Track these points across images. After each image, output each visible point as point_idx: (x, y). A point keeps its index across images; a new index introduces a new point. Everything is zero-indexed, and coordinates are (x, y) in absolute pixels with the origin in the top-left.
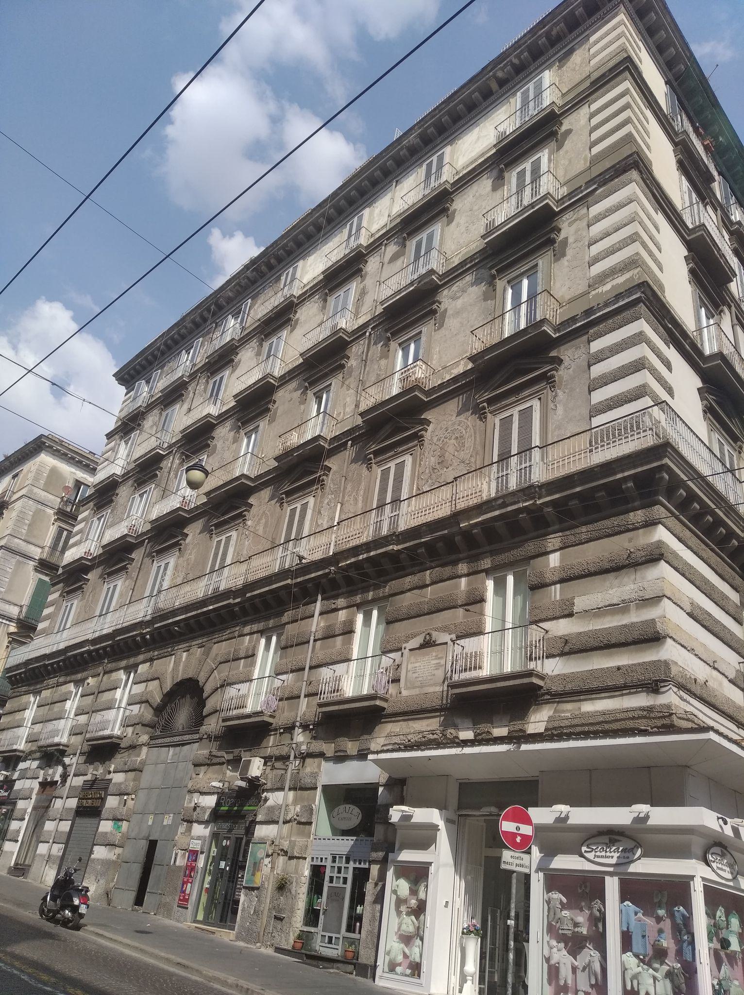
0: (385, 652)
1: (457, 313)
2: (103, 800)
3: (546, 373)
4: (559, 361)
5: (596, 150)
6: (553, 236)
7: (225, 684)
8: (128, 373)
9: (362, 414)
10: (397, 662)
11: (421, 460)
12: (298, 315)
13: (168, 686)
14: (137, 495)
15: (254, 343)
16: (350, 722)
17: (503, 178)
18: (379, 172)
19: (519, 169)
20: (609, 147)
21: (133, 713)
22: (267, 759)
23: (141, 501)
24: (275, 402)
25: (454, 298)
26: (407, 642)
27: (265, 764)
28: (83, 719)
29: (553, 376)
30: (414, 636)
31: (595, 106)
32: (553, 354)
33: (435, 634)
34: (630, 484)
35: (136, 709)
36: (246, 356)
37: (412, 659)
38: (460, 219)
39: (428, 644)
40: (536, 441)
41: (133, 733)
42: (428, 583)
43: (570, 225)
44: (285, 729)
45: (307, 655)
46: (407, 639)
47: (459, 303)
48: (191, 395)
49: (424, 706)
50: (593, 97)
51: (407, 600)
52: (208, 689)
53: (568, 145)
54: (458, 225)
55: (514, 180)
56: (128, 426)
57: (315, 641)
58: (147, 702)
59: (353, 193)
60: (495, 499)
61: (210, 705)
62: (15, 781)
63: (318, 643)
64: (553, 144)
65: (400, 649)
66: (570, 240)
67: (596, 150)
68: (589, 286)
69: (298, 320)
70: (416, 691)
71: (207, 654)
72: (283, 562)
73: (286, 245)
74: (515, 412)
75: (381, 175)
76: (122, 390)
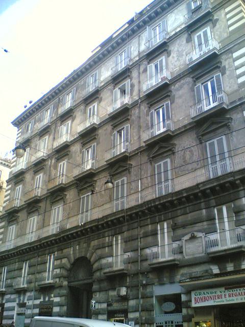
0: (125, 252)
1: (180, 97)
2: (52, 309)
3: (226, 124)
4: (175, 145)
5: (231, 29)
6: (219, 65)
7: (101, 258)
8: (18, 121)
9: (5, 211)
10: (180, 245)
11: (174, 161)
12: (101, 95)
13: (72, 260)
14: (84, 150)
15: (82, 107)
16: (167, 270)
17: (191, 37)
18: (159, 9)
19: (197, 34)
20: (239, 27)
21: (58, 273)
22: (127, 287)
23: (121, 135)
24: (98, 135)
25: (178, 90)
26: (183, 237)
27: (127, 289)
28: (9, 281)
29: (229, 125)
30: (186, 234)
31: (227, 10)
32: (228, 116)
33: (196, 234)
34: (209, 191)
35: (58, 271)
36: (78, 115)
37: (187, 244)
38: (174, 55)
39: (193, 238)
40: (163, 180)
41: (59, 281)
42: (188, 212)
43: (226, 60)
44: (134, 275)
45: (140, 243)
46: (184, 235)
47: (180, 92)
48: (53, 131)
49: (196, 262)
50: (226, 5)
51: (180, 220)
52: (92, 260)
53: (218, 26)
54: (173, 57)
55: (196, 39)
56: (24, 145)
57: (140, 238)
58: (63, 267)
59: (68, 82)
60: (115, 213)
61: (95, 266)
62: (4, 304)
63: (142, 239)
64: (210, 24)
65: (181, 240)
66: (227, 67)
67: (231, 29)
68: (239, 87)
69: (102, 97)
70: (191, 257)
71: (89, 246)
72: (117, 208)
73: (59, 88)
74: (162, 163)
75: (154, 15)
76: (16, 128)
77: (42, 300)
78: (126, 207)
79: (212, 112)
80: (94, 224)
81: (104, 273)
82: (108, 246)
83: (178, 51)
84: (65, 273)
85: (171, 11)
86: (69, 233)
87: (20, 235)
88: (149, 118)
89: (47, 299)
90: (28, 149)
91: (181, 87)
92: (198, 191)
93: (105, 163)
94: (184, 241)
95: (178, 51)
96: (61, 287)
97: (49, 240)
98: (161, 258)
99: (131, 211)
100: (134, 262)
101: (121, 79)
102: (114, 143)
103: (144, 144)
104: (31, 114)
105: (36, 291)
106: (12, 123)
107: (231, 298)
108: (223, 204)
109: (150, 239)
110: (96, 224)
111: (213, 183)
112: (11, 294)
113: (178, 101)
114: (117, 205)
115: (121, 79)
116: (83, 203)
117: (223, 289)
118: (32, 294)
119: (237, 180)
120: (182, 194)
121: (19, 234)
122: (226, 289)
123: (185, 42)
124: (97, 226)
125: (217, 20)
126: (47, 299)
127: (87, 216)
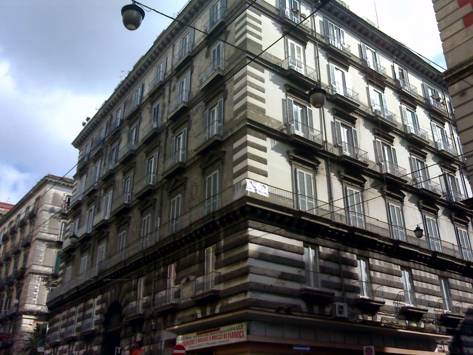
13: (109, 303)
25: (194, 114)
26: (182, 280)
57: (155, 282)
66: (229, 91)
77: (84, 350)
78: (218, 207)
81: (156, 310)
82: (134, 290)
83: (199, 67)
85: (199, 17)
87: (76, 273)
88: (172, 145)
89: (89, 349)
90: (84, 177)
91: (197, 111)
93: (195, 153)
94: (182, 284)
95: (199, 67)
96: (99, 334)
102: (148, 171)
103: (194, 154)
104: (153, 59)
105: (81, 340)
106: (72, 144)
107: (226, 339)
109: (161, 282)
112: (64, 344)
113: (194, 127)
114: (209, 207)
116: (120, 242)
117: (195, 334)
122: (198, 334)
123: (204, 57)
125: (229, 31)
126: (89, 349)
127: (214, 204)
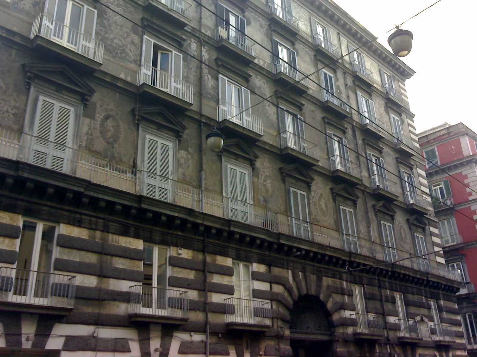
61: (336, 317)
79: (68, 55)
80: (76, 189)
84: (287, 314)
86: (296, 245)
92: (227, 229)
96: (279, 337)
97: (155, 209)
98: (15, 293)
99: (334, 252)
100: (98, 300)
101: (363, 87)
108: (42, 219)
110: (82, 190)
111: (294, 243)
115: (363, 87)
118: (198, 337)
119: (87, 196)
120: (416, 274)
121: (285, 214)
124: (78, 196)
